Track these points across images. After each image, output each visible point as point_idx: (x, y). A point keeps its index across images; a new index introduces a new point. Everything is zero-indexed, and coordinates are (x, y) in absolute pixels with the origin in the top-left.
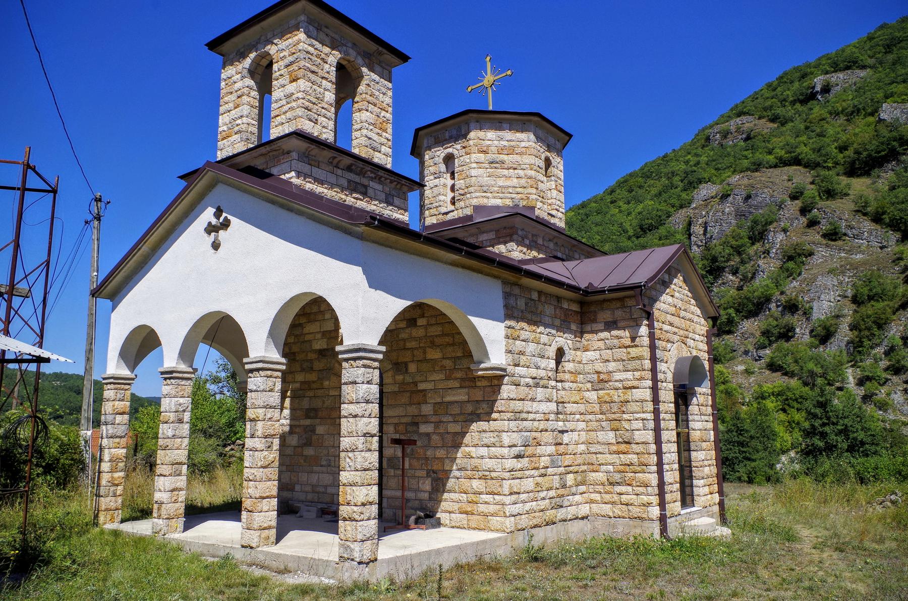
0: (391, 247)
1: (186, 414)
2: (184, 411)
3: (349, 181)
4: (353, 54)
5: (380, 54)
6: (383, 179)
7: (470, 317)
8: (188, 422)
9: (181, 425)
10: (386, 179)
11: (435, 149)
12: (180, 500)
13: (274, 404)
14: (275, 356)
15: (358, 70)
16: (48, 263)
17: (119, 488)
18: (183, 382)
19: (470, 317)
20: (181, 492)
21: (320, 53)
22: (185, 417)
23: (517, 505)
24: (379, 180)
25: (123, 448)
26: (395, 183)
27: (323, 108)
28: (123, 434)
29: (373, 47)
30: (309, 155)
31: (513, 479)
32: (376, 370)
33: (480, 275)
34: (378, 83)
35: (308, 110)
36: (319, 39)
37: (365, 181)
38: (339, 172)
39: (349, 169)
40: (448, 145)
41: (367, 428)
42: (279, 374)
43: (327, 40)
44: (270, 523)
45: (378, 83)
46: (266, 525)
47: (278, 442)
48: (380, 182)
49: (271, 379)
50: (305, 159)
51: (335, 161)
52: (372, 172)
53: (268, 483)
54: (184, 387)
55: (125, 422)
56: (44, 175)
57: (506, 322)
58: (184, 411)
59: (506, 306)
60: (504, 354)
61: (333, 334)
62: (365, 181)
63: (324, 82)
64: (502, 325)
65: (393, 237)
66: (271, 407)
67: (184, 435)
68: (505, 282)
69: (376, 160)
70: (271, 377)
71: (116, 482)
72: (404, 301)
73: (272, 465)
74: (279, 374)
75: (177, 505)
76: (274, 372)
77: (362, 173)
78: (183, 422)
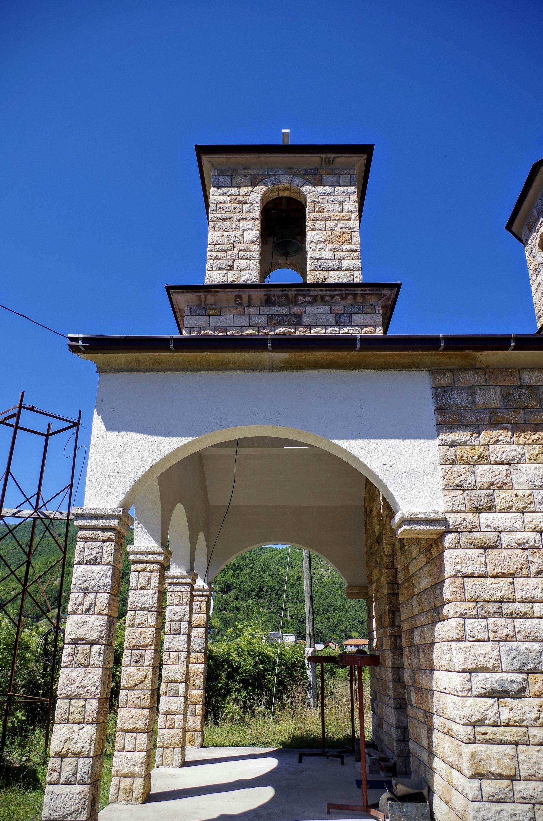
0: (151, 370)
1: (182, 623)
2: (181, 620)
3: (270, 317)
4: (284, 180)
5: (329, 162)
6: (327, 298)
7: (334, 441)
8: (184, 634)
9: (177, 637)
10: (332, 297)
11: (530, 240)
12: (176, 725)
13: (147, 606)
14: (150, 545)
15: (301, 194)
16: (71, 486)
17: (198, 706)
18: (180, 588)
19: (334, 441)
20: (177, 716)
21: (234, 197)
22: (182, 627)
23: (507, 807)
24: (314, 301)
25: (200, 663)
26: (351, 297)
27: (240, 250)
28: (199, 649)
29: (314, 159)
30: (206, 305)
31: (488, 742)
32: (107, 544)
33: (363, 371)
34: (330, 194)
35: (219, 260)
36: (234, 184)
37: (296, 310)
38: (254, 310)
39: (268, 302)
40: (539, 225)
41: (80, 631)
42: (156, 567)
43: (245, 180)
44: (132, 769)
45: (330, 194)
46: (125, 771)
47: (152, 656)
48: (325, 303)
49: (143, 574)
50: (200, 311)
51: (245, 301)
52: (304, 296)
53: (133, 710)
54: (180, 593)
55: (201, 635)
56: (55, 413)
57: (443, 436)
58: (181, 620)
59: (440, 410)
60: (441, 493)
61: (391, 511)
62: (296, 310)
63: (242, 223)
64: (437, 442)
65: (145, 357)
66: (141, 610)
67: (181, 648)
68: (434, 370)
69: (332, 281)
70: (143, 570)
71: (194, 700)
72: (172, 439)
73: (141, 686)
74: (156, 567)
75: (172, 732)
76: (148, 565)
77: (289, 302)
78: (179, 633)
